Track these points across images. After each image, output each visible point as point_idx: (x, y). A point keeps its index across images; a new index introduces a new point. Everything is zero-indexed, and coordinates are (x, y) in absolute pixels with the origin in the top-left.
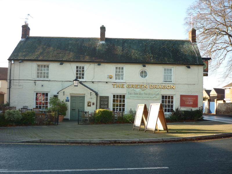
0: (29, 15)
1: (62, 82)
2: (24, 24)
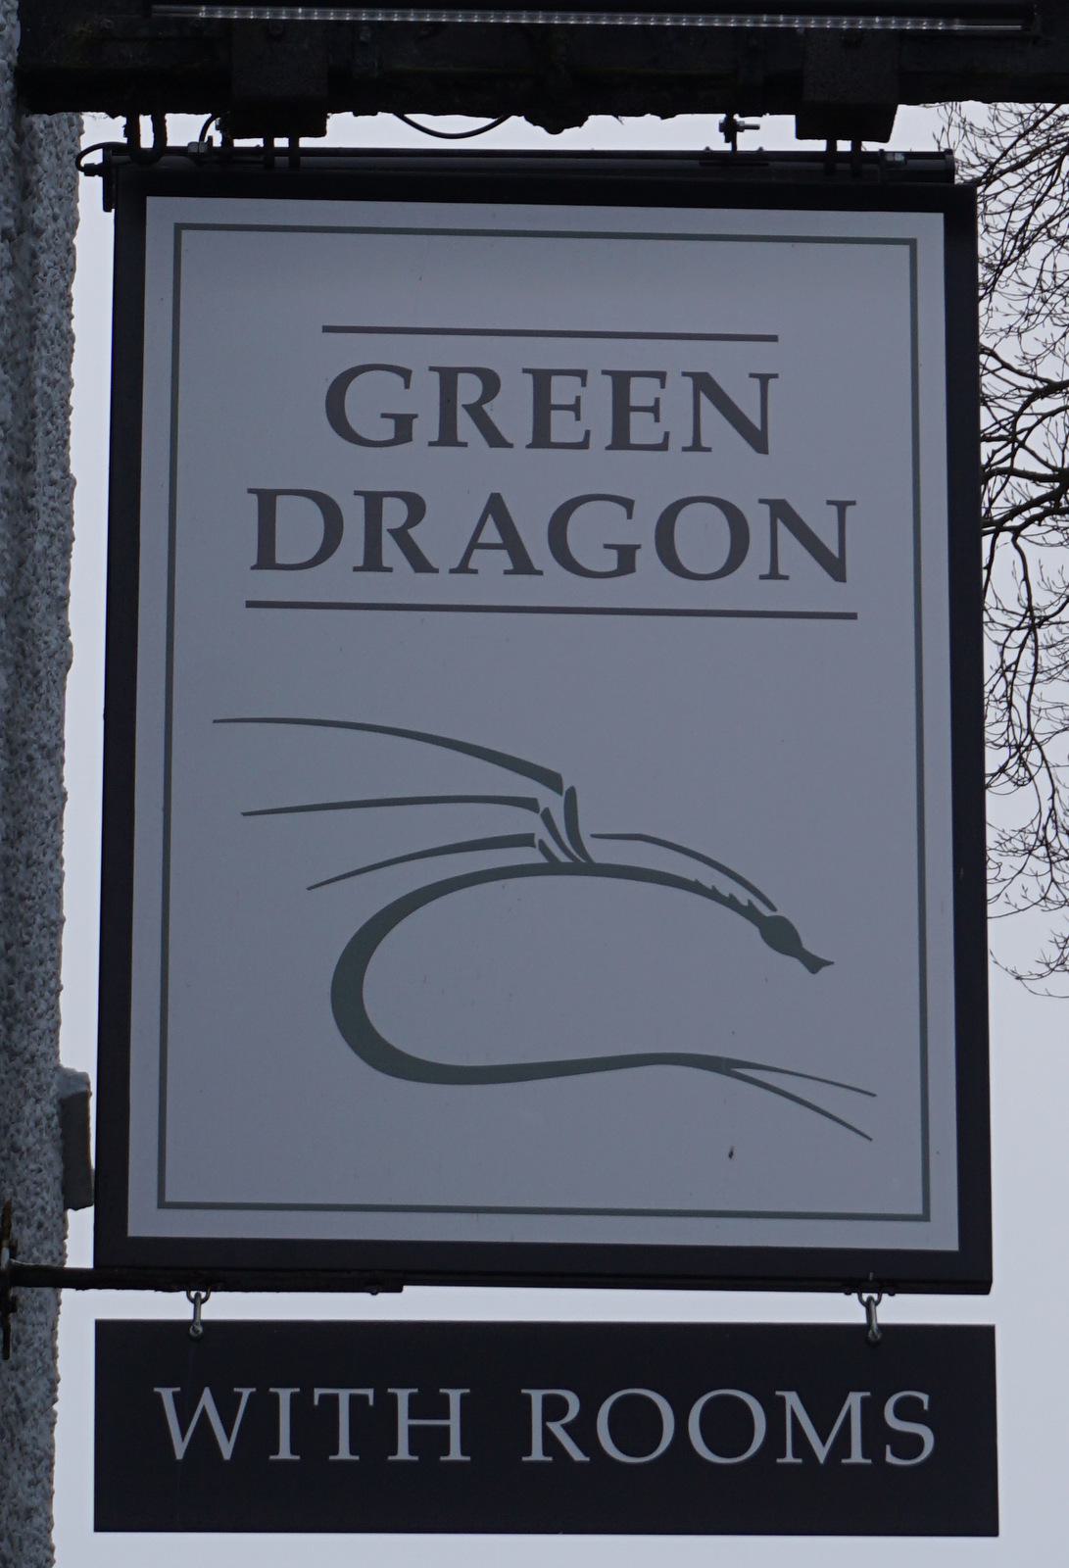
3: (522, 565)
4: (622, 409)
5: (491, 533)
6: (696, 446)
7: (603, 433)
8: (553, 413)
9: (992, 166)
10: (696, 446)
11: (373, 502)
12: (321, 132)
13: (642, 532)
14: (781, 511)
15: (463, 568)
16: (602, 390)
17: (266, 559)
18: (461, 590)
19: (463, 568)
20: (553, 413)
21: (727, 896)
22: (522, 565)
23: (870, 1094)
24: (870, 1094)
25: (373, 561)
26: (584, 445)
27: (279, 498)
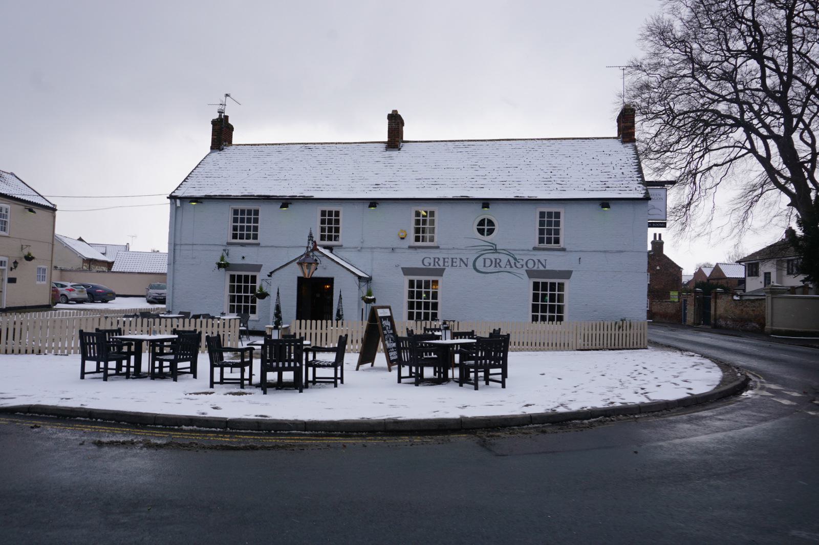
0: (227, 95)
1: (287, 249)
2: (216, 116)
3: (511, 267)
4: (452, 262)
5: (508, 264)
6: (460, 266)
7: (450, 265)
8: (115, 368)
9: (689, 58)
10: (460, 266)
11: (496, 259)
12: (121, 370)
13: (524, 263)
14: (539, 261)
15: (505, 267)
16: (450, 260)
17: (485, 266)
18: (505, 270)
19: (505, 267)
20: (115, 368)
21: (487, 336)
22: (511, 267)
23: (14, 338)
24: (14, 338)
25: (496, 266)
26: (456, 266)
27: (95, 370)
